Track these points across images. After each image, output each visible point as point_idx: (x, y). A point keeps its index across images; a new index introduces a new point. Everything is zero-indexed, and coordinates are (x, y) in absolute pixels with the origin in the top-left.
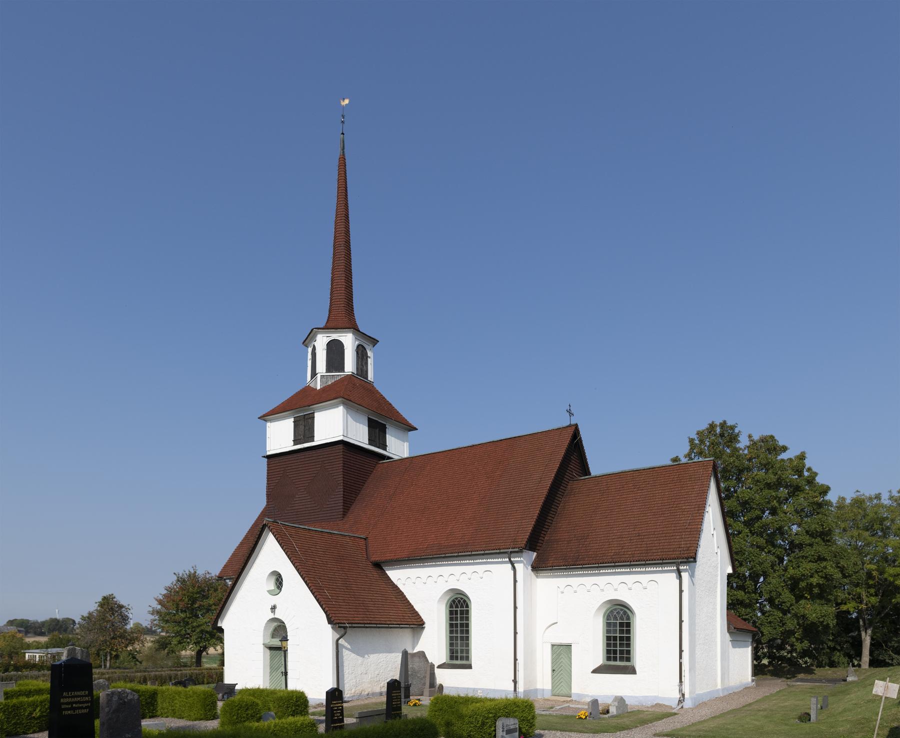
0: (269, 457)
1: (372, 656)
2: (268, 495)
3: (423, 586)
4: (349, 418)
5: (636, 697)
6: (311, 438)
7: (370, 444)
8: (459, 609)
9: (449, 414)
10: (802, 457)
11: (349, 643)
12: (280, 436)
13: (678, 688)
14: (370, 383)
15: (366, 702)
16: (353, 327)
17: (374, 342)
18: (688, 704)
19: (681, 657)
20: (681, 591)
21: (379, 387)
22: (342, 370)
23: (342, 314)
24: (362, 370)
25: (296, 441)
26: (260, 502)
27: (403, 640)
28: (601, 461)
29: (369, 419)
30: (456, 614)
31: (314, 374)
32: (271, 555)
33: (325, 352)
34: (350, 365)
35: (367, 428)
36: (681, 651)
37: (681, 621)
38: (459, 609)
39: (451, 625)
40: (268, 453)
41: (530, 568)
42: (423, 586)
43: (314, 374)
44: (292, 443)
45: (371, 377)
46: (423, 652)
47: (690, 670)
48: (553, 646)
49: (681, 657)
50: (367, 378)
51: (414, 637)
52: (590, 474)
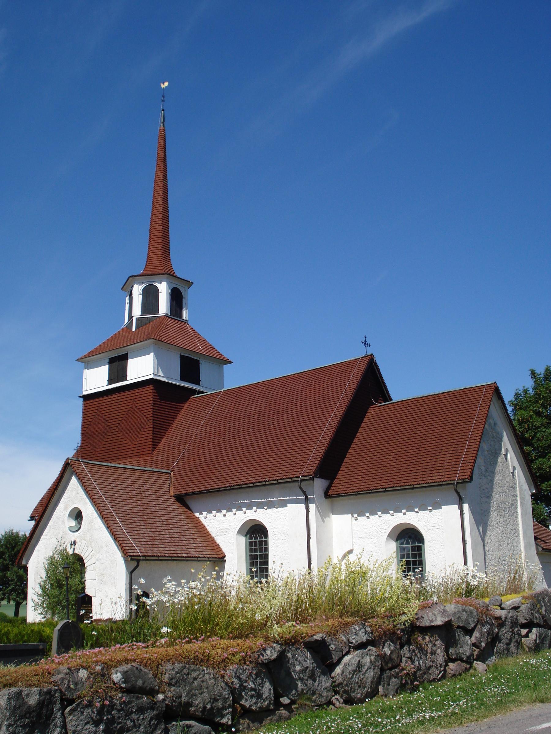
0: (86, 398)
2: (84, 434)
3: (224, 526)
6: (125, 378)
7: (183, 379)
8: (256, 534)
9: (259, 348)
10: (533, 374)
12: (97, 379)
16: (170, 275)
17: (189, 284)
22: (157, 312)
23: (159, 262)
25: (110, 382)
26: (76, 440)
28: (402, 386)
29: (181, 355)
30: (256, 545)
31: (131, 317)
32: (74, 495)
34: (163, 308)
38: (256, 534)
39: (251, 557)
40: (84, 393)
42: (224, 526)
43: (131, 317)
44: (107, 383)
52: (391, 400)
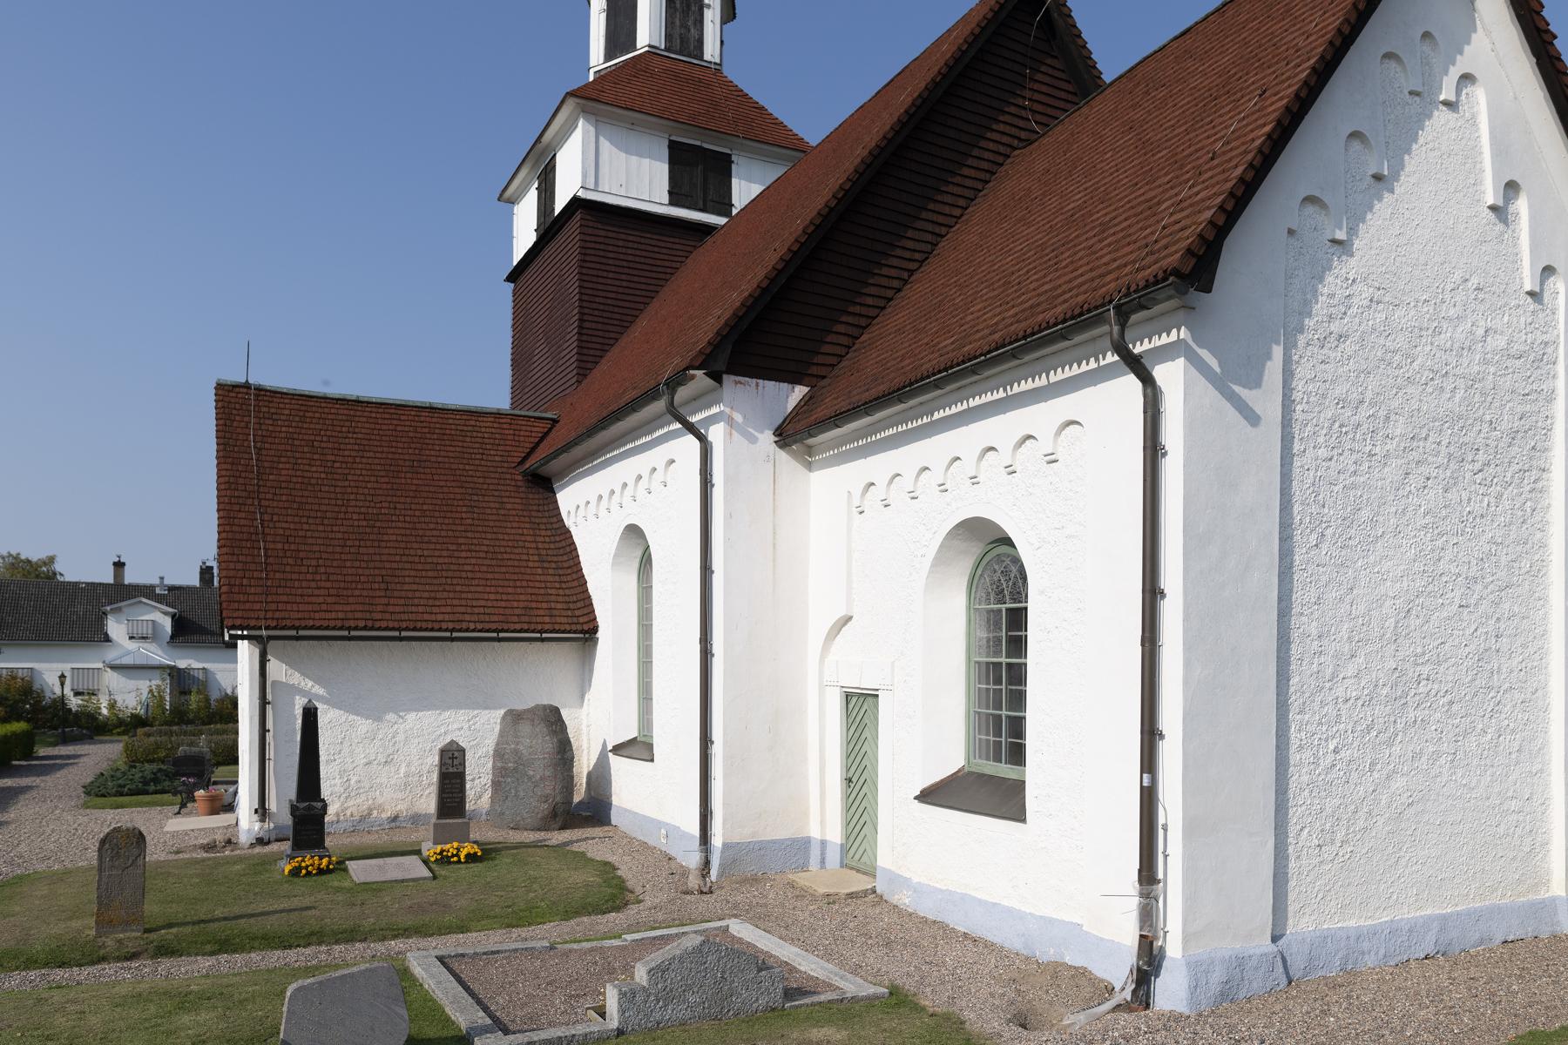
1: (411, 716)
4: (605, 144)
5: (1021, 916)
7: (672, 203)
11: (317, 681)
13: (1134, 902)
14: (717, 69)
15: (347, 841)
18: (1170, 992)
19: (1149, 762)
20: (1153, 450)
21: (731, 73)
24: (684, 40)
27: (534, 674)
33: (604, 16)
35: (666, 167)
36: (1150, 734)
37: (1152, 593)
41: (767, 438)
45: (711, 51)
46: (556, 711)
47: (225, 946)
48: (848, 696)
49: (1149, 762)
50: (701, 58)
51: (583, 664)
